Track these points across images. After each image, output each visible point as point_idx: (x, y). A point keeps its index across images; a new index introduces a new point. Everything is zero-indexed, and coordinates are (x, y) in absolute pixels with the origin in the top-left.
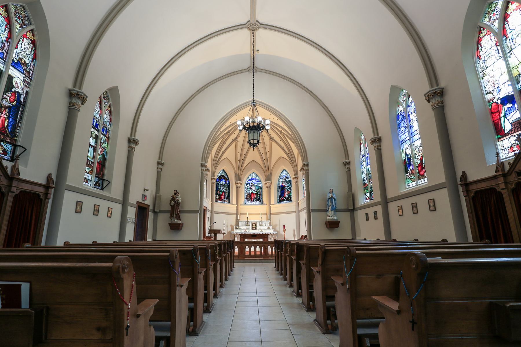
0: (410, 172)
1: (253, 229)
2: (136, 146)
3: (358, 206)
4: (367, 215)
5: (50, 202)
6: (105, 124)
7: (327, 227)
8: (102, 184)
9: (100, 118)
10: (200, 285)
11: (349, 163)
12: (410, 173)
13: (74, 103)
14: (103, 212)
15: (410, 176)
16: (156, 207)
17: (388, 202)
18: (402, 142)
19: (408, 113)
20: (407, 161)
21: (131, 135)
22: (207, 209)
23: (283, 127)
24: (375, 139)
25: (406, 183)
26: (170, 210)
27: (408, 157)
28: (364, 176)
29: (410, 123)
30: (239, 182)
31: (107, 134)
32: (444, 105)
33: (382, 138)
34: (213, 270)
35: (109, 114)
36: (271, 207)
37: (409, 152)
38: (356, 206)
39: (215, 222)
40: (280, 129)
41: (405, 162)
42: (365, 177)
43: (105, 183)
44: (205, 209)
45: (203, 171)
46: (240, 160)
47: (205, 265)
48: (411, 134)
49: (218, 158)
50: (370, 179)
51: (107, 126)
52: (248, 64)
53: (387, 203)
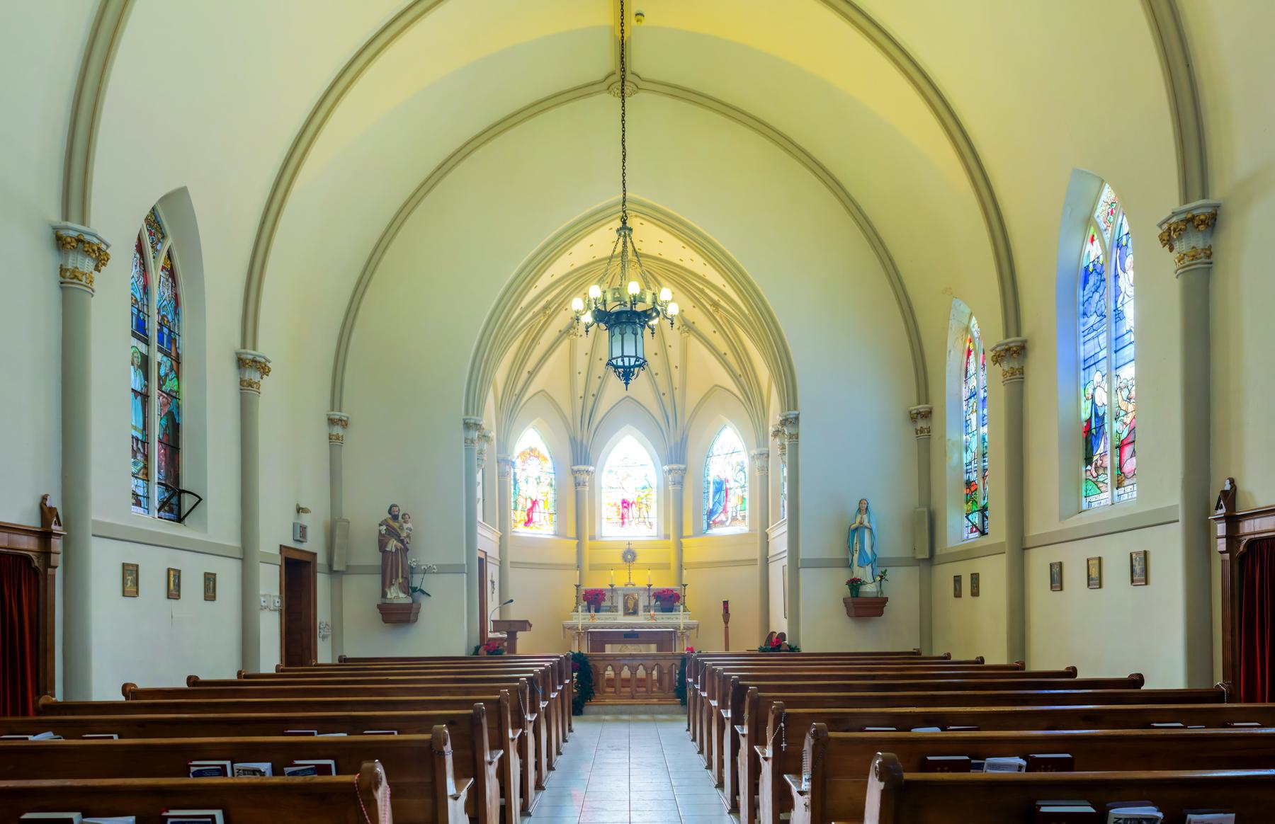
0: (1097, 460)
1: (627, 613)
2: (262, 378)
3: (944, 552)
4: (958, 580)
5: (58, 573)
6: (163, 316)
7: (848, 614)
8: (179, 505)
9: (147, 300)
10: (491, 791)
11: (927, 415)
12: (1096, 464)
13: (73, 272)
14: (192, 586)
15: (1095, 474)
16: (336, 558)
17: (1028, 546)
18: (1089, 363)
19: (1116, 269)
20: (1093, 426)
21: (244, 346)
22: (490, 557)
23: (723, 288)
24: (1006, 347)
25: (1084, 494)
26: (380, 563)
27: (1096, 414)
28: (969, 458)
29: (1116, 302)
30: (582, 467)
31: (173, 349)
32: (1211, 263)
33: (1028, 346)
34: (517, 751)
35: (170, 280)
36: (684, 545)
37: (1101, 397)
38: (938, 552)
39: (512, 601)
40: (716, 298)
41: (1088, 430)
42: (971, 463)
43: (187, 501)
44: (483, 556)
45: (472, 442)
46: (584, 398)
47: (499, 742)
48: (1116, 339)
49: (517, 392)
50: (985, 470)
51: (168, 321)
52: (605, 62)
53: (1024, 549)
